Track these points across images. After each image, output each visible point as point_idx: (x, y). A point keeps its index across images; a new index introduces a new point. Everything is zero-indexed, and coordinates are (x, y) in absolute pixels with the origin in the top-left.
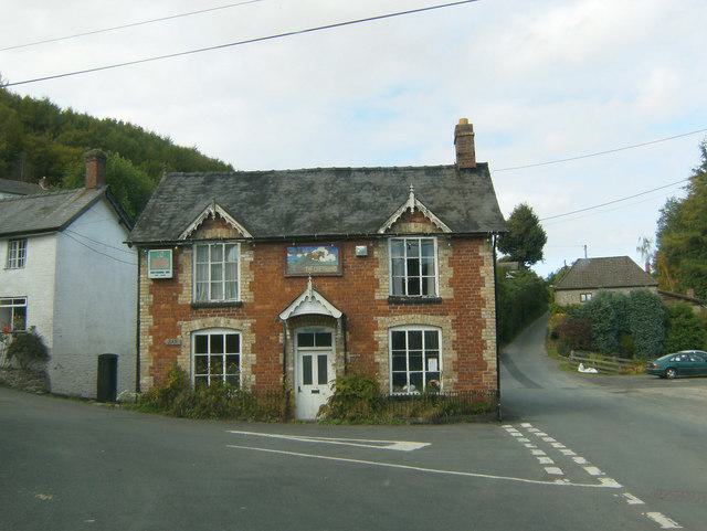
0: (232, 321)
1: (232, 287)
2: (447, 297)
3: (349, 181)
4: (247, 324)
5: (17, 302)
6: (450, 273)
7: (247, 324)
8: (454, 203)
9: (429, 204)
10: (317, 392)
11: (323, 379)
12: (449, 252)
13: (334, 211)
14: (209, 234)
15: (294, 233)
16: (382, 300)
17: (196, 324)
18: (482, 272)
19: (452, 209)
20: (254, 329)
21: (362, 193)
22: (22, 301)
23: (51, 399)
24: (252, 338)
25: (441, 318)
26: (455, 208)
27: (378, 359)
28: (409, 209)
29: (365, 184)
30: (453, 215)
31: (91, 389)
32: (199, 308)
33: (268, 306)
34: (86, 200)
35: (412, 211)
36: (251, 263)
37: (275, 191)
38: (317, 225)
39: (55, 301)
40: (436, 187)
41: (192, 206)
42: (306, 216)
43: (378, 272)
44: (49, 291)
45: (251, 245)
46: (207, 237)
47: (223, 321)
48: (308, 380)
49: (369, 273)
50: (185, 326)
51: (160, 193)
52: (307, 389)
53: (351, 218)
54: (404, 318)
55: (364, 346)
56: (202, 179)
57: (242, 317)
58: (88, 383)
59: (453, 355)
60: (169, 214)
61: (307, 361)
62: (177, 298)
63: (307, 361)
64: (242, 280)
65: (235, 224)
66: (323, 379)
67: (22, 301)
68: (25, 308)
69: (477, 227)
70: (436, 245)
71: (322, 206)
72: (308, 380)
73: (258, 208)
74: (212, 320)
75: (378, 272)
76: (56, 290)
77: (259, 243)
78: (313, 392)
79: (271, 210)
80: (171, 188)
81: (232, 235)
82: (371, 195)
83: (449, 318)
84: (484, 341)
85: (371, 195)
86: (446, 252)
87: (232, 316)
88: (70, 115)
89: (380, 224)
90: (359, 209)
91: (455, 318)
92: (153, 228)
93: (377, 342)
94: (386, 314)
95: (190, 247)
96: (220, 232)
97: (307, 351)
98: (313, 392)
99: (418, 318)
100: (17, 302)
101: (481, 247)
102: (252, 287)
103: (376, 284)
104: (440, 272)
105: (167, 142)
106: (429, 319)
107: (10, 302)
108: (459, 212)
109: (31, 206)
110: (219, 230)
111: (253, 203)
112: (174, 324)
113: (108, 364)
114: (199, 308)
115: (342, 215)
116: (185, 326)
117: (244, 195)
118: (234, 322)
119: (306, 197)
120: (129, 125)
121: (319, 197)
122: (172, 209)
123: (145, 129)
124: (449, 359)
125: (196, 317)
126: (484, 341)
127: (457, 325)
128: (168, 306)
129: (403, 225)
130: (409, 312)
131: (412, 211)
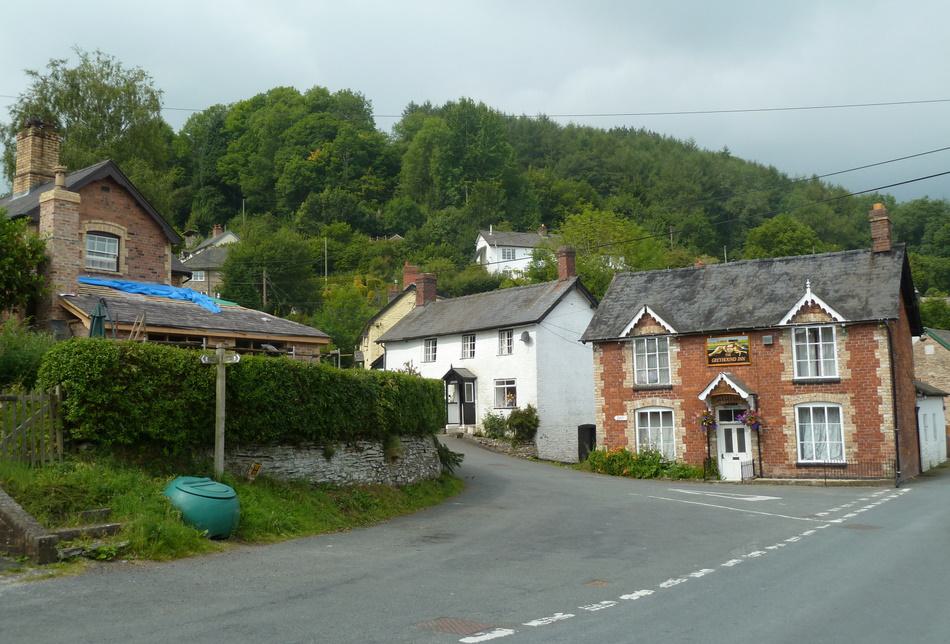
0: (665, 400)
1: (664, 372)
2: (846, 377)
3: (769, 273)
4: (678, 403)
5: (508, 383)
6: (847, 356)
7: (678, 403)
8: (858, 291)
9: (822, 295)
10: (738, 458)
11: (742, 449)
12: (846, 338)
13: (748, 304)
14: (644, 331)
15: (710, 328)
16: (788, 381)
17: (638, 403)
18: (877, 355)
19: (853, 297)
20: (682, 407)
21: (779, 284)
22: (513, 382)
23: (540, 463)
24: (682, 415)
25: (841, 396)
26: (857, 295)
27: (786, 432)
28: (807, 302)
29: (782, 275)
30: (852, 304)
31: (572, 454)
32: (639, 391)
33: (692, 388)
34: (563, 289)
35: (810, 304)
36: (678, 353)
37: (703, 287)
38: (732, 319)
39: (538, 381)
40: (846, 274)
41: (634, 305)
42: (725, 309)
43: (783, 358)
44: (533, 373)
45: (677, 338)
46: (643, 333)
47: (658, 401)
48: (729, 449)
49: (776, 359)
50: (629, 405)
51: (610, 293)
52: (729, 457)
53: (764, 310)
54: (806, 397)
55: (774, 420)
56: (645, 278)
57: (673, 398)
58: (570, 448)
59: (853, 428)
60: (615, 314)
61: (728, 433)
62: (622, 383)
63: (728, 433)
64: (673, 366)
65: (663, 323)
66: (742, 449)
67: (513, 382)
68: (514, 389)
69: (870, 313)
70: (834, 332)
71: (739, 300)
72: (729, 449)
73: (687, 304)
74: (650, 400)
75: (783, 358)
76: (538, 373)
77: (685, 337)
78: (734, 458)
79: (697, 305)
80: (619, 288)
81: (662, 331)
82: (784, 286)
83: (849, 396)
84: (881, 416)
85: (784, 286)
86: (843, 338)
87: (665, 396)
88: (572, 132)
89: (782, 316)
90: (771, 301)
91: (853, 395)
92: (603, 326)
93: (784, 417)
94: (791, 393)
95: (629, 342)
96: (654, 330)
97: (727, 425)
98: (734, 458)
99: (820, 396)
100: (508, 383)
101: (875, 332)
102: (680, 373)
103: (781, 367)
104: (839, 356)
105: (689, 149)
106: (829, 397)
107: (503, 383)
108: (859, 300)
109: (516, 298)
110: (652, 327)
111: (684, 299)
112: (621, 403)
113: (587, 433)
114: (639, 391)
115: (754, 308)
116: (629, 405)
117: (677, 293)
118: (667, 402)
119: (730, 291)
120: (642, 132)
121: (738, 292)
122: (618, 308)
123: (661, 135)
124: (849, 432)
125: (637, 398)
126: (881, 416)
127: (855, 401)
128: (616, 389)
129: (804, 316)
130: (812, 391)
131: (810, 304)
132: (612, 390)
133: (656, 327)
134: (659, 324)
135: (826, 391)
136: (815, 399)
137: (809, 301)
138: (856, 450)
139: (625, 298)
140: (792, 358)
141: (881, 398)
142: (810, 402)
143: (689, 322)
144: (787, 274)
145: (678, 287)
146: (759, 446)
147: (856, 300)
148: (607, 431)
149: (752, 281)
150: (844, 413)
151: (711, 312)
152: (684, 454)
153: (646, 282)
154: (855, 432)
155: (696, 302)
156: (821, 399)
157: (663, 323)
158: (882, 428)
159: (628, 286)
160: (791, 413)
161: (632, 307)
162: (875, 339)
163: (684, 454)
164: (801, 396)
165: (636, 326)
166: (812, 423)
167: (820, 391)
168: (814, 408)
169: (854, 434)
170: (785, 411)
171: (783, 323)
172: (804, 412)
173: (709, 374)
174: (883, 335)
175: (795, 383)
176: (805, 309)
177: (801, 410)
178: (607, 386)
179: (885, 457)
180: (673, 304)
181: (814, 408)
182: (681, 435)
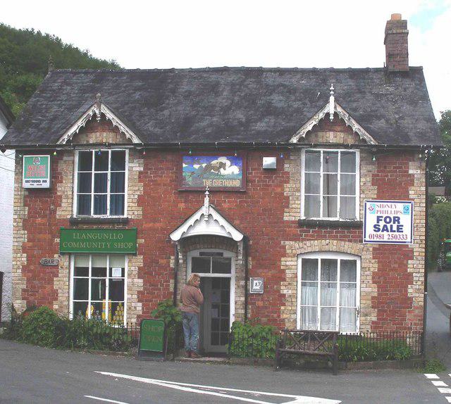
16: (293, 222)
27: (284, 291)
30: (381, 124)
32: (310, 228)
33: (158, 225)
35: (332, 117)
36: (140, 173)
37: (173, 91)
45: (141, 152)
62: (55, 211)
65: (123, 128)
71: (226, 110)
75: (288, 189)
84: (411, 274)
86: (370, 167)
89: (294, 131)
93: (284, 271)
94: (296, 238)
102: (141, 201)
103: (284, 202)
104: (362, 191)
108: (387, 121)
114: (310, 228)
117: (137, 96)
128: (44, 220)
129: (320, 134)
130: (324, 237)
131: (332, 117)
132: (39, 220)
133: (111, 135)
134: (116, 130)
135: (342, 239)
136: (327, 248)
137: (332, 112)
138: (375, 319)
139: (64, 97)
140: (299, 190)
141: (412, 251)
142: (320, 252)
143: (158, 130)
144: (283, 85)
145: (137, 89)
146: (246, 309)
147: (383, 120)
148: (29, 281)
149: (239, 90)
150: (362, 268)
151: (188, 122)
152: (138, 317)
153: (93, 81)
154: (376, 295)
155: (165, 108)
156: (334, 248)
157: (123, 128)
158: (410, 291)
159: (68, 84)
160: (294, 266)
161: (75, 108)
162: (411, 172)
163: (138, 317)
164: (308, 243)
165: (82, 129)
166: (319, 281)
167: (335, 238)
168: (341, 260)
169: (373, 298)
170: (286, 262)
171: (294, 140)
172: (309, 265)
173: (182, 206)
174: (420, 168)
175: (301, 224)
176: (325, 124)
177: (305, 262)
178: (33, 214)
179: (410, 329)
180: (134, 108)
181: (341, 260)
182: (136, 289)
